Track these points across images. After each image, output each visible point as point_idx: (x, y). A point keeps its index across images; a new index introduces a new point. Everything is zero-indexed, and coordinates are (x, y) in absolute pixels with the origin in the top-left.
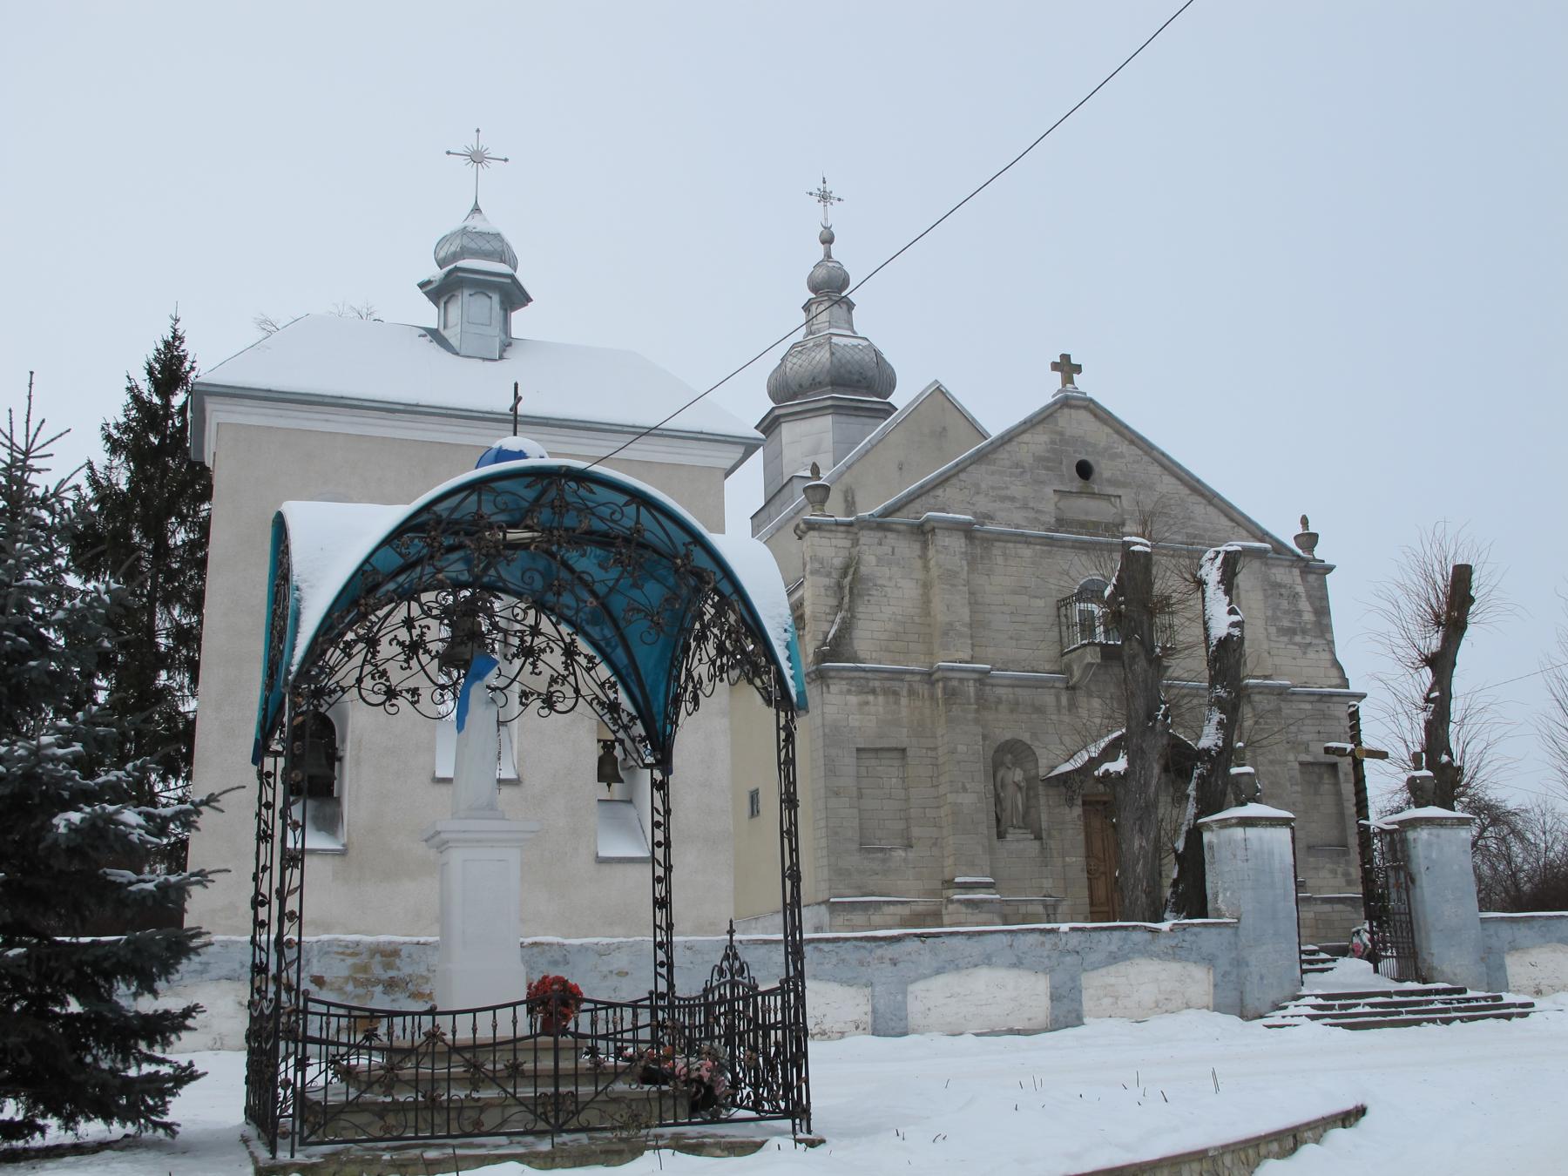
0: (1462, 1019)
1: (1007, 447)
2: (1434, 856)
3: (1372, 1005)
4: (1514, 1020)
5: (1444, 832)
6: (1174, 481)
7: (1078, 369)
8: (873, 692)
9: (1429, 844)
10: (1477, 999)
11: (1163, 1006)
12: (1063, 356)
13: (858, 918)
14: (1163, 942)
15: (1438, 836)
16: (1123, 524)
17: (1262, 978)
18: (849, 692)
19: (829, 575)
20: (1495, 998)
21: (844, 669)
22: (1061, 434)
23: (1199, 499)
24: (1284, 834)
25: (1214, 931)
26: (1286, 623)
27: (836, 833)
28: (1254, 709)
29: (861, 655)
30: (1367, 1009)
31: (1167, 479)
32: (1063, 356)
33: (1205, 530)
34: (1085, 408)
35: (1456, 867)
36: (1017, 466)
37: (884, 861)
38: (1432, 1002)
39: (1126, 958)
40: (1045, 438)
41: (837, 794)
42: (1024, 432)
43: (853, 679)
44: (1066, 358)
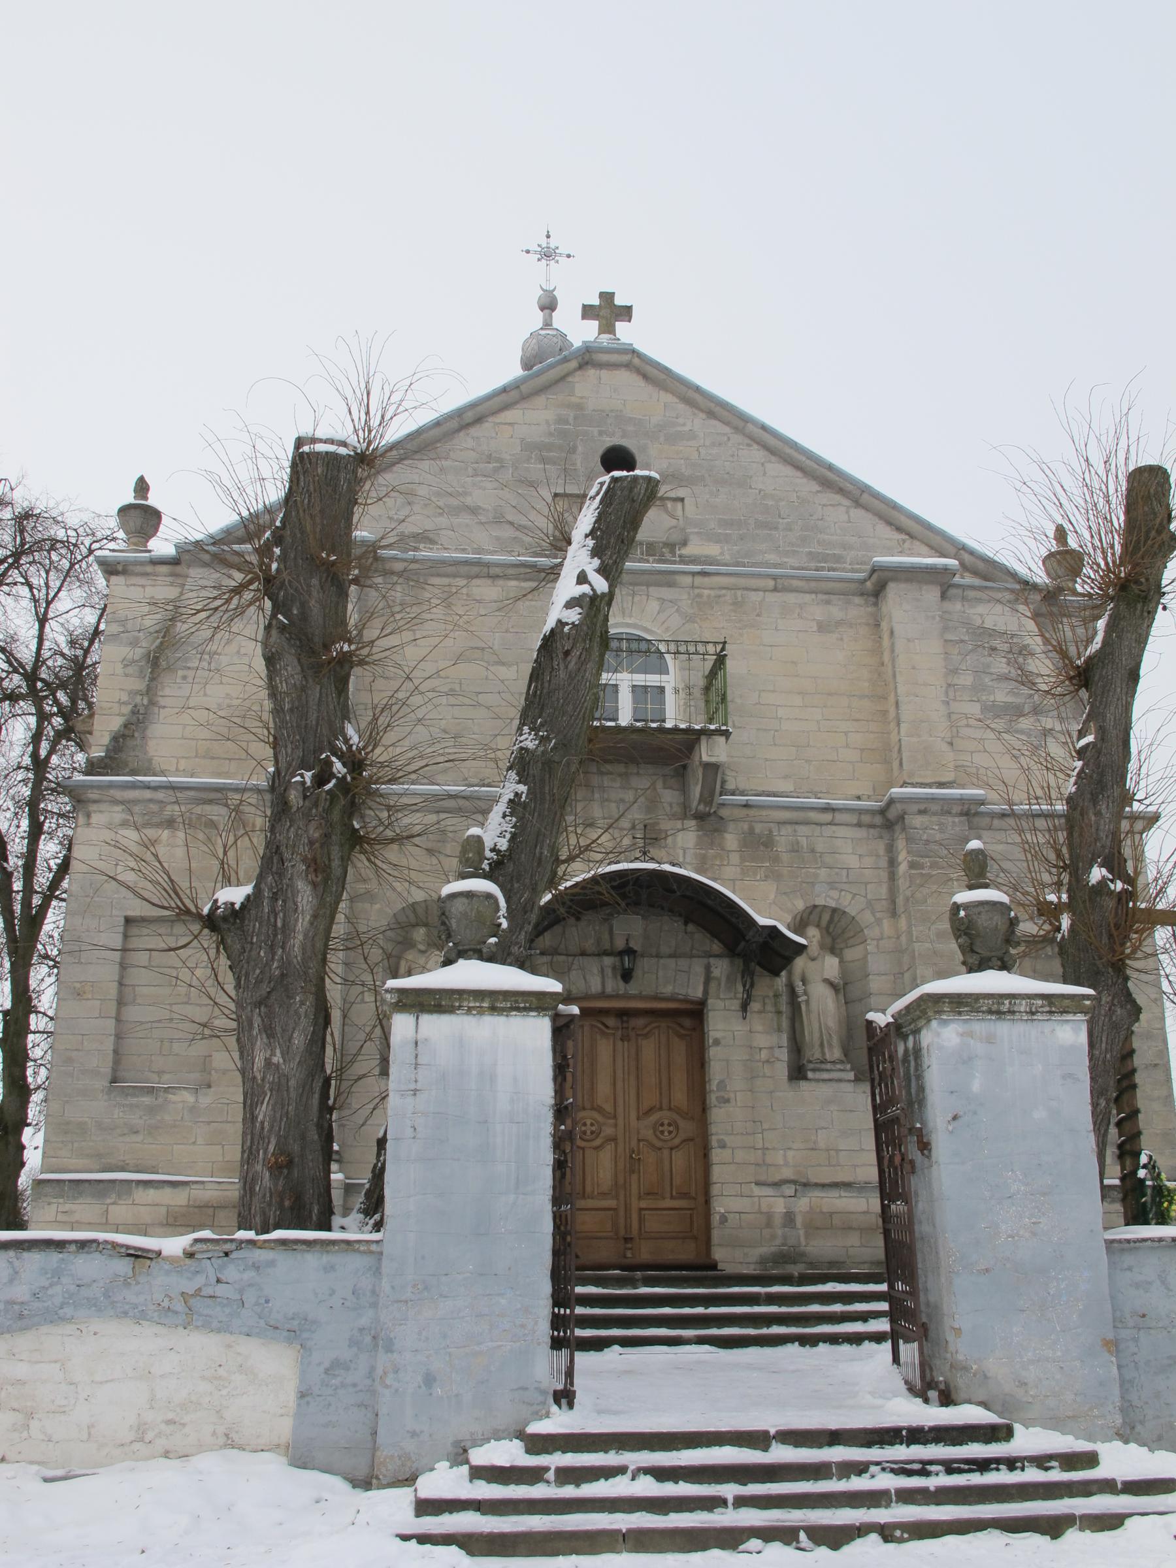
0: (887, 1533)
1: (474, 431)
2: (976, 1086)
3: (662, 1474)
4: (1073, 1537)
5: (1004, 1029)
6: (789, 471)
7: (626, 313)
8: (170, 823)
9: (965, 1059)
10: (1041, 1461)
11: (158, 1440)
12: (628, 309)
13: (85, 1208)
14: (160, 1282)
15: (990, 1040)
16: (684, 543)
17: (429, 1380)
18: (124, 824)
19: (134, 643)
20: (1070, 1461)
21: (111, 785)
22: (579, 407)
23: (838, 498)
24: (537, 1032)
25: (312, 1260)
26: (1002, 695)
27: (69, 1060)
28: (909, 840)
29: (159, 762)
30: (647, 1487)
31: (777, 468)
32: (628, 309)
33: (845, 546)
34: (628, 366)
35: (1039, 1114)
36: (489, 459)
37: (151, 1110)
38: (860, 1468)
39: (54, 1317)
40: (550, 415)
41: (79, 994)
42: (506, 407)
43: (136, 802)
44: (607, 297)
